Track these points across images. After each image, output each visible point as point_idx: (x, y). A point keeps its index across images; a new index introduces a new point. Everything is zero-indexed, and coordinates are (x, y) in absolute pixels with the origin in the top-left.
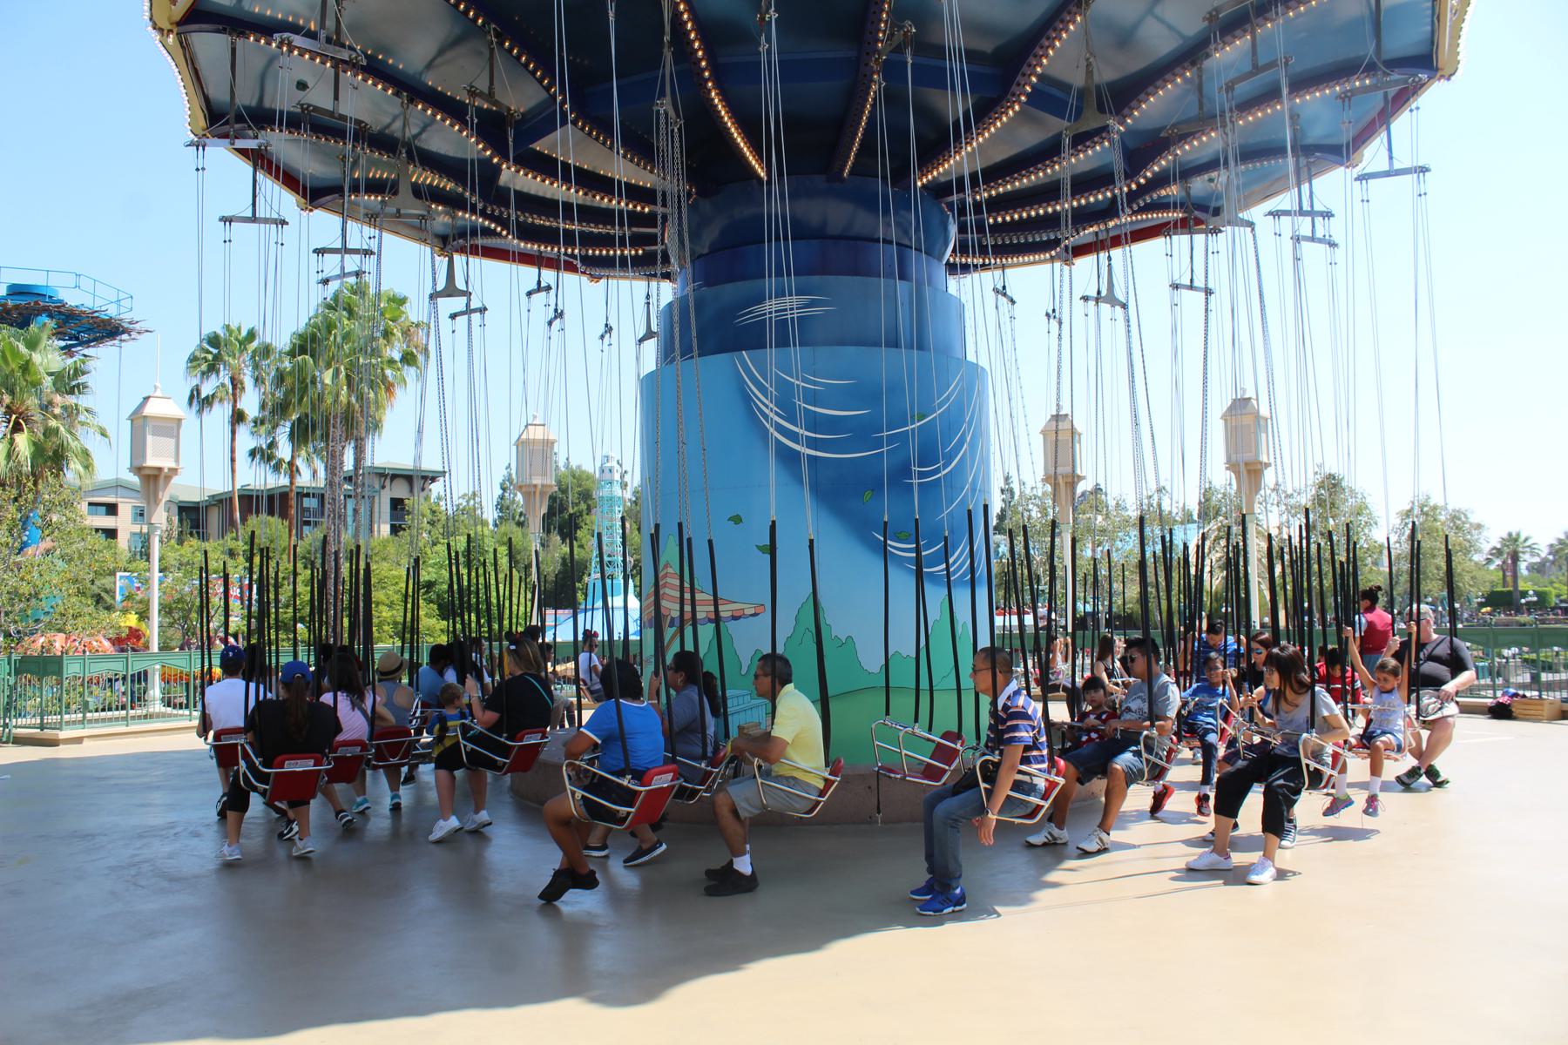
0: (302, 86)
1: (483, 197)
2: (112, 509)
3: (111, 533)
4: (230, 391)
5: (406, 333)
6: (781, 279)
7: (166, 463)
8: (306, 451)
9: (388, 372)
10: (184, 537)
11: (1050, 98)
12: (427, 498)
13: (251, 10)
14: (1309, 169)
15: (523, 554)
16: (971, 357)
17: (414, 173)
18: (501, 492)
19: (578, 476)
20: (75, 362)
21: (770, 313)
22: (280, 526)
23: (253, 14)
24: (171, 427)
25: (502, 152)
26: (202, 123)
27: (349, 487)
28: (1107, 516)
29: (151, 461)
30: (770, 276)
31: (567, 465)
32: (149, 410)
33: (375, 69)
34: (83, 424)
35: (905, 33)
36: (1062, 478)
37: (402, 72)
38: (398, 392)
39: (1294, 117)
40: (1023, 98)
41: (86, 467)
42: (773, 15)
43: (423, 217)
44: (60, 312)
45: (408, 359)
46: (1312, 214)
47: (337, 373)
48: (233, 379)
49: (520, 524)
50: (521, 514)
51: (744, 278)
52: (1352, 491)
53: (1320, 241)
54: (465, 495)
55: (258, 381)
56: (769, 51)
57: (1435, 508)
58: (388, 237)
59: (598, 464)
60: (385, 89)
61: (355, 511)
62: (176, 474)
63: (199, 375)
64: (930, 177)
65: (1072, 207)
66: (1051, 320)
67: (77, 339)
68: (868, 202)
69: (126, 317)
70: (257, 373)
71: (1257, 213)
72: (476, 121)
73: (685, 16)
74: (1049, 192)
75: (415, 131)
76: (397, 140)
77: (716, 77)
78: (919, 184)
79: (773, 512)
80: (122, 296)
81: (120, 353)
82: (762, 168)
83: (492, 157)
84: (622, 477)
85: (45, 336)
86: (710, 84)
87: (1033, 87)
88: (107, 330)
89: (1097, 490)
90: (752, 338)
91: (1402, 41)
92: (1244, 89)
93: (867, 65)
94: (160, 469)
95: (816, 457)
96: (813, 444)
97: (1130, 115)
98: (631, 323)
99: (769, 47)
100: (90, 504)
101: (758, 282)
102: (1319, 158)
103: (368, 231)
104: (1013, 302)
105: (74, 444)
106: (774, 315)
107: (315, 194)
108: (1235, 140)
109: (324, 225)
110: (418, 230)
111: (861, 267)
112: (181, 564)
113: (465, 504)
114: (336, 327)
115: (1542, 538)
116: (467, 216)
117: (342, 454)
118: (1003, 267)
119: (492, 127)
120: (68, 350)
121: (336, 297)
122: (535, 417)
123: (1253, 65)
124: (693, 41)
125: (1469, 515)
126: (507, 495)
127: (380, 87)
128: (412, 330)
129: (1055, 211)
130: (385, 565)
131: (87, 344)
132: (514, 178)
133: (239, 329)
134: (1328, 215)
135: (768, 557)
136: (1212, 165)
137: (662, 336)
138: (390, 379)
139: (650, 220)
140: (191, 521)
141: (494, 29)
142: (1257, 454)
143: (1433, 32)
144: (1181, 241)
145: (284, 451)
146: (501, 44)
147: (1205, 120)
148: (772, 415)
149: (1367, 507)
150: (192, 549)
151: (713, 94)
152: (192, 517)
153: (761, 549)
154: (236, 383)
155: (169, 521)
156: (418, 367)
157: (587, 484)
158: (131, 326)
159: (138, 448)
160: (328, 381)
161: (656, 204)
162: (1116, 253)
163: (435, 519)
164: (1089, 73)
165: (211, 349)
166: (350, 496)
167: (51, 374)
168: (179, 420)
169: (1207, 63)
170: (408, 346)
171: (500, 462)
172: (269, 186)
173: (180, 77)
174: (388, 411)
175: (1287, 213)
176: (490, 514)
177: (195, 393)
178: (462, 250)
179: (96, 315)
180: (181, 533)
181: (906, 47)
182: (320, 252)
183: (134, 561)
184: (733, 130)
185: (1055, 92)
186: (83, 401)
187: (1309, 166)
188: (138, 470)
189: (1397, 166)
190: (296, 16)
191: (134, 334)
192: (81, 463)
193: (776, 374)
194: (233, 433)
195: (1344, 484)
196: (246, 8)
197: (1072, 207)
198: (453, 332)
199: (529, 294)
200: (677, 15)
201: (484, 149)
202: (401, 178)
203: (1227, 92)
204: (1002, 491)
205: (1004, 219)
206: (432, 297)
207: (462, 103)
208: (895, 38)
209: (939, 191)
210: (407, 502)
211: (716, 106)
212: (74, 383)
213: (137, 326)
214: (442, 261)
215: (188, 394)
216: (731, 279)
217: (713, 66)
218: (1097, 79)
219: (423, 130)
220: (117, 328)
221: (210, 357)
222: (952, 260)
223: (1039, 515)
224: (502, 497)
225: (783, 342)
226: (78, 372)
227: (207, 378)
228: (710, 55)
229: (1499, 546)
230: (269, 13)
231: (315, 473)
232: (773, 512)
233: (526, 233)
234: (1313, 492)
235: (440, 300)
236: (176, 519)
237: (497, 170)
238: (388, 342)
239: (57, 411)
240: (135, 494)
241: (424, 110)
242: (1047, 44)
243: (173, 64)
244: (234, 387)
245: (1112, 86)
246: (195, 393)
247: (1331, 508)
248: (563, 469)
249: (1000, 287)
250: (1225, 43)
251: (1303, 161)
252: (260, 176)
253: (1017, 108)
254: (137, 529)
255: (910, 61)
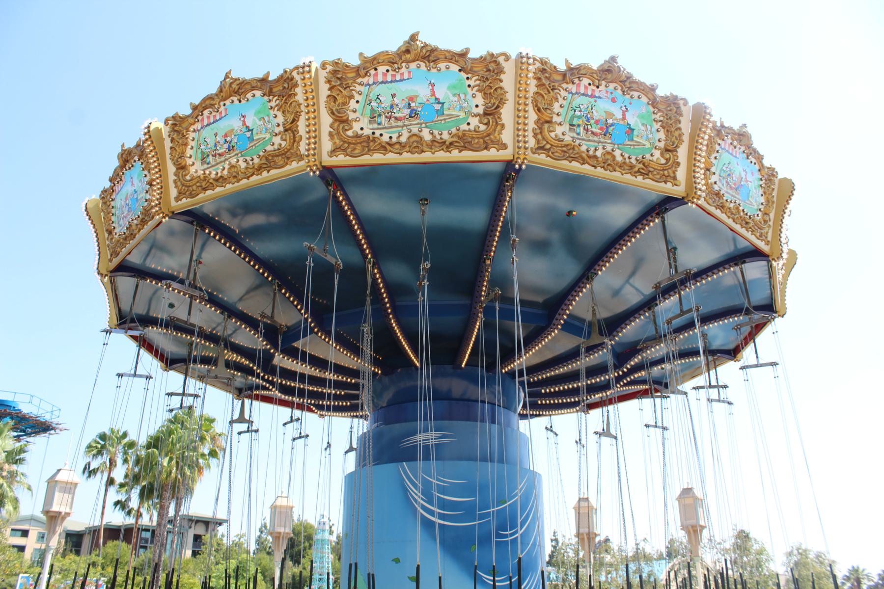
0: (171, 306)
1: (264, 370)
2: (25, 533)
3: (22, 549)
4: (108, 466)
5: (213, 439)
6: (426, 422)
7: (63, 510)
8: (148, 504)
9: (201, 461)
10: (66, 552)
11: (574, 326)
12: (216, 535)
13: (150, 266)
14: (715, 363)
15: (269, 572)
16: (531, 468)
17: (227, 354)
18: (258, 533)
19: (307, 527)
20: (21, 445)
21: (420, 441)
22: (126, 548)
23: (151, 268)
24: (70, 488)
25: (275, 346)
26: (115, 322)
27: (171, 527)
28: (613, 556)
29: (55, 508)
30: (420, 420)
31: (298, 520)
32: (59, 477)
33: (213, 301)
34: (18, 482)
35: (496, 294)
36: (586, 537)
37: (225, 301)
38: (206, 472)
39: (704, 335)
40: (559, 327)
41: (15, 508)
42: (426, 283)
43: (230, 379)
44: (18, 416)
45: (213, 454)
46: (717, 387)
47: (171, 459)
48: (110, 460)
49: (269, 553)
50: (270, 547)
51: (406, 421)
52: (755, 540)
53: (723, 402)
54: (238, 535)
55: (126, 461)
56: (423, 301)
57: (805, 551)
58: (210, 388)
59: (318, 519)
60: (216, 310)
61: (172, 542)
62: (69, 516)
63: (91, 456)
64: (509, 367)
65: (587, 384)
66: (579, 445)
67: (24, 431)
68: (473, 379)
69: (55, 421)
70: (125, 457)
71: (687, 386)
72: (263, 331)
73: (379, 280)
74: (574, 376)
75: (229, 332)
76: (219, 337)
77: (394, 312)
78: (503, 371)
79: (418, 560)
80: (55, 409)
81: (48, 441)
82: (418, 361)
83: (270, 349)
84: (331, 527)
85: (6, 430)
86: (391, 316)
87: (564, 320)
88: (43, 427)
89: (607, 540)
90: (409, 455)
91: (758, 297)
92: (677, 323)
93: (475, 308)
94: (60, 513)
95: (444, 514)
96: (442, 517)
97: (617, 335)
98: (341, 442)
99: (424, 299)
100: (12, 530)
101: (414, 423)
102: (719, 357)
103: (199, 384)
104: (556, 435)
105: (10, 494)
106: (422, 442)
107: (170, 362)
108: (674, 348)
109: (174, 379)
110: (226, 385)
111: (470, 417)
112: (61, 570)
113: (237, 540)
114: (174, 434)
115: (872, 571)
116: (254, 379)
117: (169, 507)
118: (550, 415)
119: (271, 333)
120: (18, 438)
121: (175, 417)
122: (282, 492)
123: (681, 310)
124: (383, 293)
125: (826, 555)
126: (262, 535)
127: (213, 309)
128: (216, 437)
129: (578, 386)
130: (186, 575)
131: (29, 435)
132: (280, 360)
133: (118, 431)
134: (725, 387)
135: (415, 584)
136: (661, 361)
137: (358, 451)
138: (201, 465)
139: (356, 387)
140: (73, 542)
141: (277, 283)
142: (697, 519)
143: (772, 294)
144: (647, 402)
145: (134, 503)
146: (280, 290)
147: (657, 339)
148: (419, 500)
149: (765, 550)
150: (70, 561)
151: (392, 321)
152: (75, 541)
153: (411, 579)
154: (112, 463)
155: (59, 542)
156: (218, 459)
157: (310, 531)
158: (57, 426)
159: (49, 498)
160: (165, 464)
161: (359, 378)
162: (611, 407)
163: (219, 548)
164: (594, 314)
165: (101, 442)
166: (170, 532)
167: (5, 452)
168: (76, 484)
169: (656, 309)
170: (213, 446)
171: (262, 515)
172: (145, 356)
173: (108, 301)
174: (198, 484)
175: (702, 387)
176: (253, 547)
177: (87, 466)
178: (249, 397)
179: (38, 419)
180: (65, 550)
181: (496, 301)
182: (170, 394)
183: (33, 567)
184: (402, 340)
185: (576, 323)
186: (21, 468)
187: (714, 361)
188: (46, 512)
189: (761, 362)
190: (172, 269)
191: (58, 431)
192: (13, 506)
193: (422, 476)
194: (106, 491)
195: (751, 536)
196: (147, 265)
197: (587, 384)
198: (239, 442)
199: (285, 424)
200: (374, 280)
201: (267, 345)
202: (220, 359)
203: (668, 325)
204: (552, 540)
205: (550, 390)
206: (230, 422)
207: (256, 319)
208: (490, 295)
209: (512, 374)
210: (203, 537)
211: (394, 327)
212: (17, 458)
213: (60, 426)
214: (238, 404)
215: (83, 467)
216: (398, 421)
217: (393, 307)
218: (598, 316)
219: (234, 332)
220: (49, 427)
221: (99, 446)
222: (521, 412)
223: (574, 555)
224: (259, 537)
225: (427, 458)
226: (22, 450)
227: (97, 457)
228: (392, 301)
229: (848, 574)
230: (159, 268)
231: (151, 517)
232: (418, 560)
233: (285, 390)
234: (733, 541)
235: (234, 424)
236: (63, 541)
237: (272, 356)
238: (202, 443)
239: (5, 474)
240: (41, 525)
241: (236, 322)
242: (571, 298)
243: (105, 290)
244: (111, 464)
245: (606, 320)
246: (87, 466)
247: (744, 551)
248: (296, 521)
249: (549, 427)
250: (665, 299)
251: (710, 358)
252: (142, 351)
253: (556, 331)
254: (38, 546)
255: (498, 308)
